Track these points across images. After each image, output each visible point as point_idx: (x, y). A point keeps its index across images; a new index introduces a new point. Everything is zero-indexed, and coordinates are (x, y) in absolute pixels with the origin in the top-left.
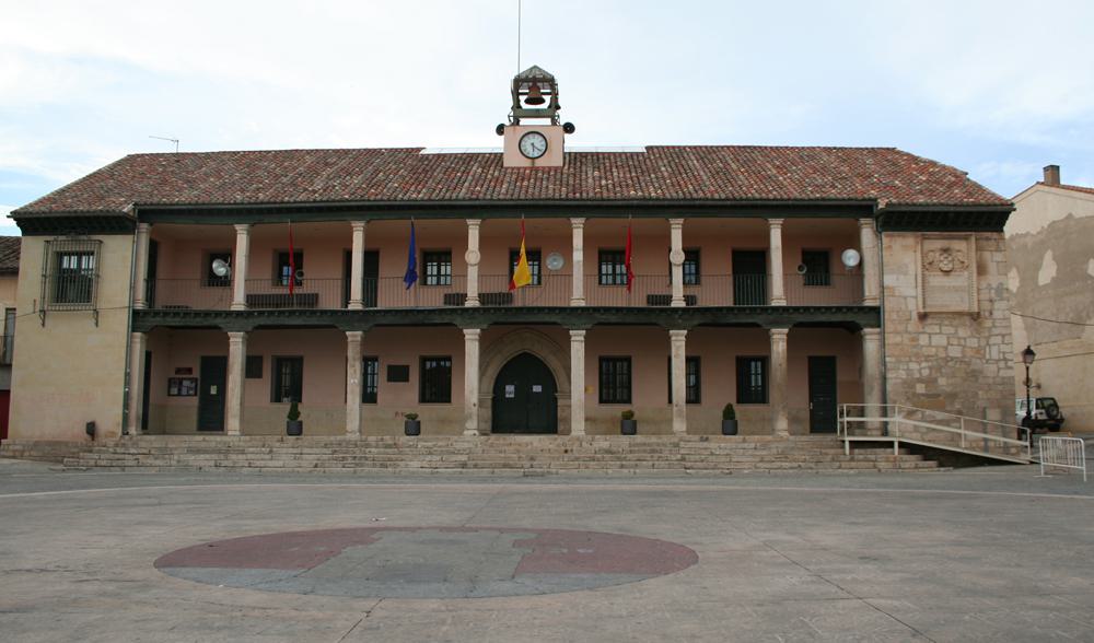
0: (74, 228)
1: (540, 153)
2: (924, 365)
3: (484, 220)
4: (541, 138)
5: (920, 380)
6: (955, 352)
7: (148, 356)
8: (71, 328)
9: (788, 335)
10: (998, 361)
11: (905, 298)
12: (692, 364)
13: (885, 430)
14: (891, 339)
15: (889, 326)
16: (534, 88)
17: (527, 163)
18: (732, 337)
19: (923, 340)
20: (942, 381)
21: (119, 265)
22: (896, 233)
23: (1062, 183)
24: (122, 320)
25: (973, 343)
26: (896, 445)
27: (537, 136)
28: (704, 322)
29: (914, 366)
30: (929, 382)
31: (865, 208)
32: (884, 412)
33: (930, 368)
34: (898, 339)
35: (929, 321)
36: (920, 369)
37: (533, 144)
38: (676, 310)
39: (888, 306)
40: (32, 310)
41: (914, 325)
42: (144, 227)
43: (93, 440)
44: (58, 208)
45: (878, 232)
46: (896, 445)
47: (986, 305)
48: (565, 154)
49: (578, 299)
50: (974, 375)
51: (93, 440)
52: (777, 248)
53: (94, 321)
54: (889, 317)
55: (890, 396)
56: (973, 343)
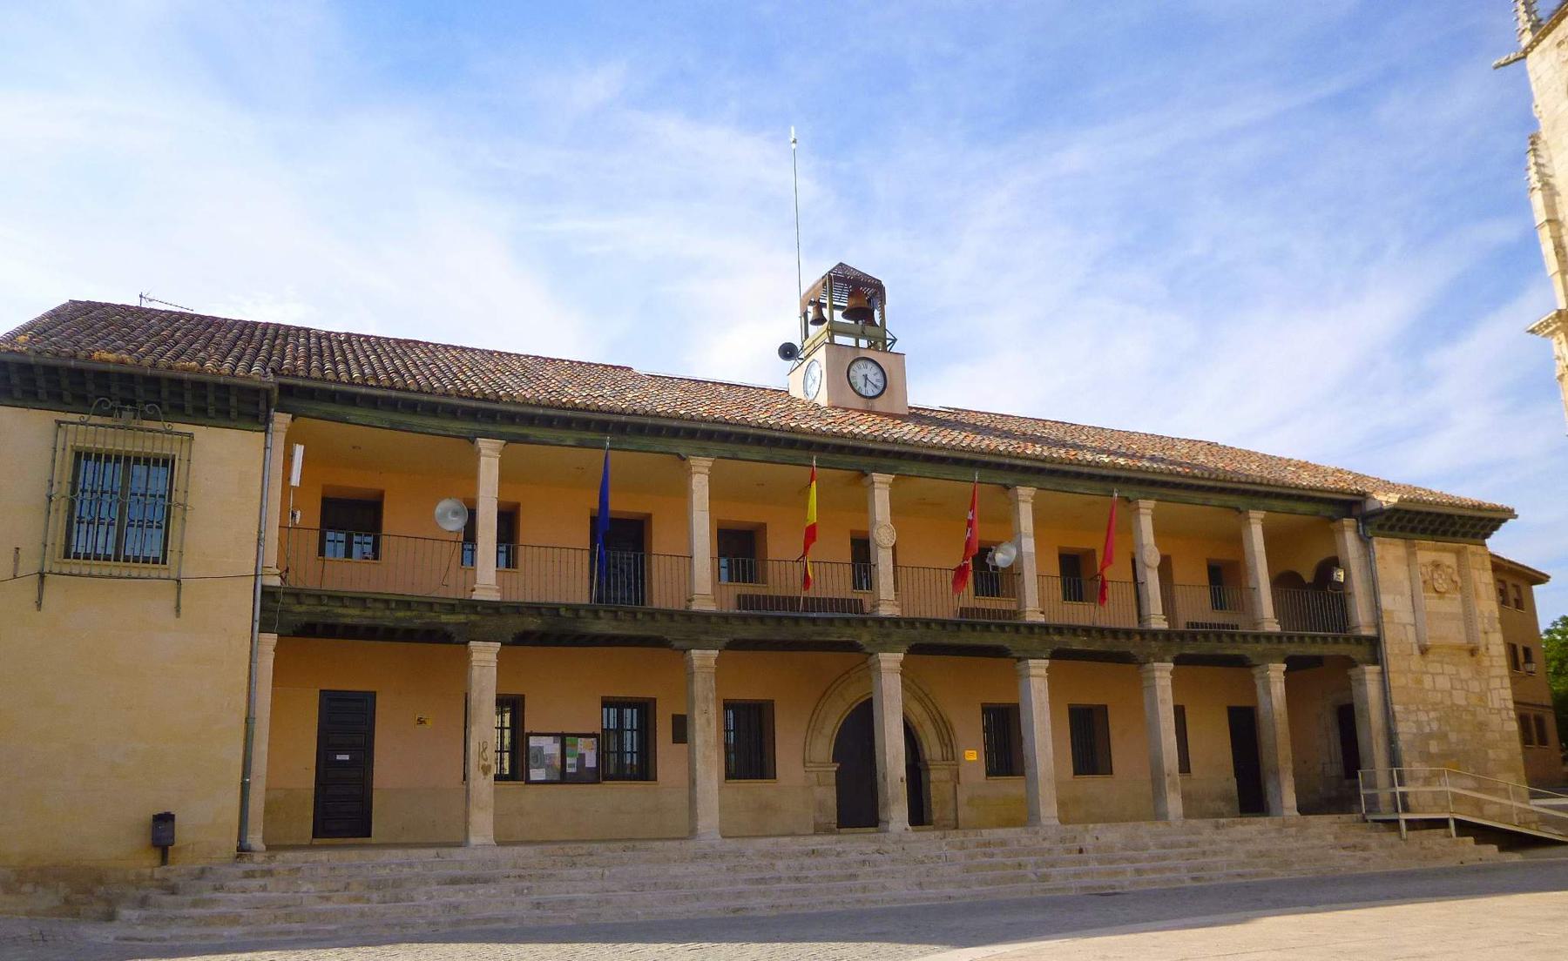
0: (133, 403)
1: (877, 392)
2: (1432, 714)
3: (901, 476)
4: (875, 369)
5: (1431, 736)
7: (1180, 712)
8: (109, 616)
9: (1048, 670)
10: (1499, 711)
11: (1404, 626)
14: (1396, 681)
15: (1394, 662)
16: (856, 299)
19: (1427, 682)
20: (1453, 737)
21: (235, 489)
22: (1387, 540)
24: (242, 606)
25: (1475, 686)
26: (1452, 823)
27: (870, 365)
28: (537, 632)
29: (1423, 717)
30: (1443, 737)
33: (1439, 719)
34: (1403, 681)
35: (1430, 657)
36: (1430, 721)
37: (866, 377)
39: (1389, 634)
41: (1416, 662)
42: (281, 421)
43: (164, 860)
45: (1365, 541)
46: (1452, 823)
47: (1482, 642)
48: (266, 431)
50: (1482, 726)
51: (164, 860)
52: (1029, 554)
53: (34, 596)
54: (1391, 649)
56: (1475, 686)
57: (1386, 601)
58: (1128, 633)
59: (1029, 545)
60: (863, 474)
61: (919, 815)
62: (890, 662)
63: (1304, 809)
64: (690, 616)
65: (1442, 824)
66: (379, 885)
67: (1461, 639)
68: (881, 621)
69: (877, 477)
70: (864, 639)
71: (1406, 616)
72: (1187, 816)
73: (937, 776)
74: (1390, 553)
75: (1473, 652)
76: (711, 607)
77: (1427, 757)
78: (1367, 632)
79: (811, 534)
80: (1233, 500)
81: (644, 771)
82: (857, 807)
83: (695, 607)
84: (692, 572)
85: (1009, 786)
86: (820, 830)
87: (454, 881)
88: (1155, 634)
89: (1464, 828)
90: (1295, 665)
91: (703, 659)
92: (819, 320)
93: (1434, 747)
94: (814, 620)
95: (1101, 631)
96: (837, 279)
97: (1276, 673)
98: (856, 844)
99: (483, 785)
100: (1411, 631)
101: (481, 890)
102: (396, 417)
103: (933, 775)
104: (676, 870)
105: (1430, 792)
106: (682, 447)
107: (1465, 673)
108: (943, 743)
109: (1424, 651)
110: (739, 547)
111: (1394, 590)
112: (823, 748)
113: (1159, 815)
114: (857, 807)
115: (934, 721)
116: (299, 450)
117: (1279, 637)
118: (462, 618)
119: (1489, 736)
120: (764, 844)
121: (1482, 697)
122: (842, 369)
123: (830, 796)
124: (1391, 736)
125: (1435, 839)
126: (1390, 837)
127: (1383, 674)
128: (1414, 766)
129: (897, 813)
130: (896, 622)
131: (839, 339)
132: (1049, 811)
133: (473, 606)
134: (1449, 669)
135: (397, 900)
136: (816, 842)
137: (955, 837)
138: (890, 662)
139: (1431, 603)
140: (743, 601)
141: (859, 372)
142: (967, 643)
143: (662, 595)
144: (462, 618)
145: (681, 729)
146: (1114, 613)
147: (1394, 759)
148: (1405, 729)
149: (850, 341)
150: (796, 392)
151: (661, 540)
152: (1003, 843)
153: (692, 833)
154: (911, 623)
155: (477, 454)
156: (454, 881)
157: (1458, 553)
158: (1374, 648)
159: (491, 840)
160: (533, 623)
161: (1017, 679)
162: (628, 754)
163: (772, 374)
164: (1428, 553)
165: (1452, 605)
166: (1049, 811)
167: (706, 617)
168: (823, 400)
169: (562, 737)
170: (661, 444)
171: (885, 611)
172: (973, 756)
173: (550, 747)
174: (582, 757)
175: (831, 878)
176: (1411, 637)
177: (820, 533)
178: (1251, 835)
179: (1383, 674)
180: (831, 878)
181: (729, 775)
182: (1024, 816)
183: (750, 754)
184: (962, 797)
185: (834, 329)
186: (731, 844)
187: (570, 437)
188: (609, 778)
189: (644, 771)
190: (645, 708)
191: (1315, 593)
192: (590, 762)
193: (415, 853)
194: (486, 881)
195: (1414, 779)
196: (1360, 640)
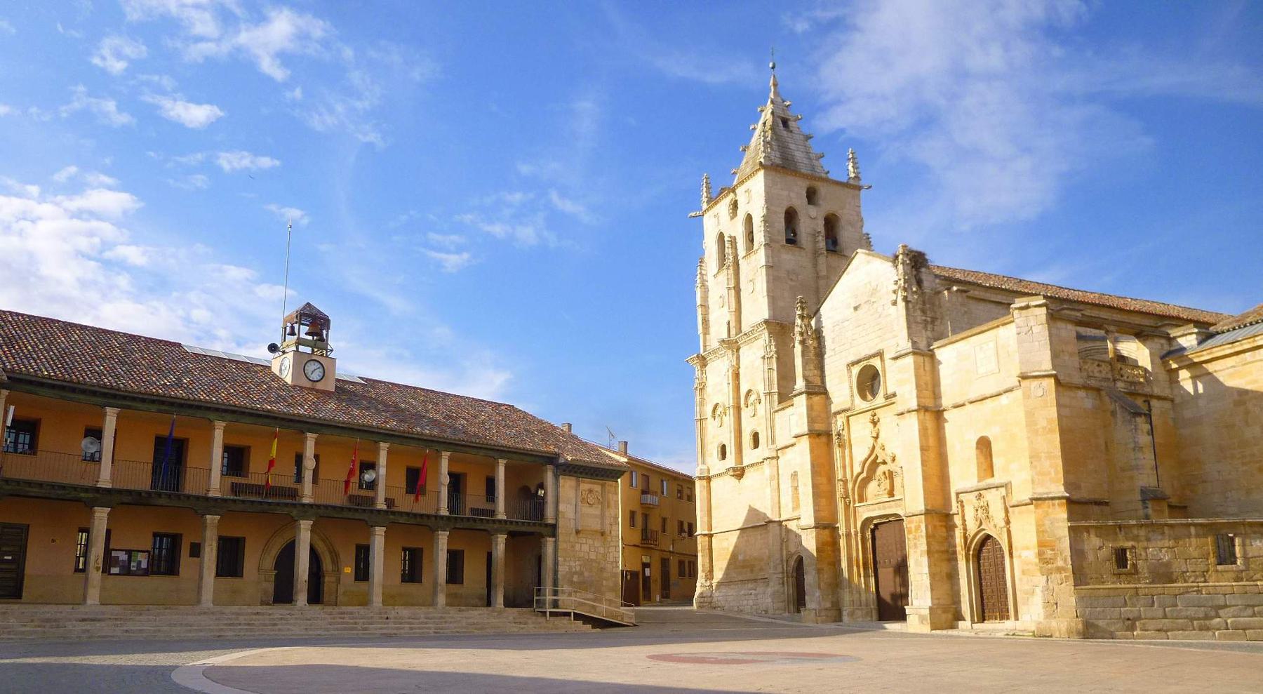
5: (576, 573)
6: (593, 556)
7: (108, 532)
12: (816, 399)
13: (555, 604)
14: (561, 545)
15: (561, 538)
17: (309, 385)
18: (471, 526)
19: (577, 547)
20: (586, 574)
23: (947, 354)
25: (602, 550)
28: (123, 501)
29: (572, 564)
30: (581, 574)
31: (552, 459)
32: (555, 593)
36: (576, 566)
38: (379, 511)
39: (561, 523)
40: (714, 483)
41: (573, 538)
44: (394, 398)
45: (556, 477)
49: (105, 479)
50: (602, 570)
54: (561, 531)
55: (560, 582)
56: (602, 550)
57: (562, 507)
58: (429, 516)
59: (382, 471)
60: (303, 432)
61: (315, 597)
62: (305, 526)
63: (506, 605)
64: (207, 499)
65: (568, 614)
66: (48, 620)
67: (598, 527)
68: (304, 505)
69: (309, 435)
70: (294, 513)
71: (571, 515)
72: (447, 604)
73: (328, 580)
74: (568, 486)
75: (603, 534)
76: (219, 495)
77: (571, 583)
78: (550, 521)
79: (271, 463)
80: (491, 453)
81: (171, 569)
82: (283, 594)
83: (211, 495)
84: (209, 473)
85: (362, 586)
86: (263, 603)
87: (84, 620)
88: (442, 517)
89: (578, 617)
90: (512, 535)
91: (212, 519)
92: (293, 333)
93: (575, 579)
94: (270, 504)
95: (415, 515)
96: (305, 315)
97: (501, 540)
98: (279, 611)
99: (95, 576)
100: (573, 522)
101: (98, 624)
102: (64, 394)
103: (327, 579)
104: (191, 619)
105: (570, 600)
106: (212, 416)
107: (597, 544)
108: (333, 562)
109: (578, 532)
110: (236, 459)
111: (566, 500)
112: (269, 562)
113: (433, 604)
114: (283, 594)
115: (330, 553)
116: (12, 408)
117: (506, 522)
118: (91, 495)
119: (605, 575)
120: (235, 609)
121: (604, 555)
122: (301, 363)
123: (270, 587)
124: (556, 572)
125: (565, 620)
126: (542, 620)
127: (556, 542)
128: (564, 587)
129: (302, 598)
130: (311, 506)
131: (302, 348)
132: (377, 599)
133: (98, 490)
134: (590, 542)
135: (58, 627)
136: (259, 609)
137: (329, 609)
138: (305, 526)
139: (586, 510)
140: (235, 489)
141: (311, 367)
142: (351, 517)
143: (191, 486)
144: (91, 495)
145: (196, 551)
146: (423, 506)
147: (555, 583)
148: (562, 569)
149: (309, 350)
150: (275, 370)
151: (193, 458)
152: (351, 613)
153: (199, 602)
154: (318, 506)
155: (105, 414)
156: (84, 620)
157: (603, 486)
158: (553, 530)
159: (97, 602)
160: (126, 499)
161: (370, 535)
162: (166, 561)
163: (260, 354)
164: (586, 485)
165: (596, 511)
166: (377, 599)
167: (216, 499)
168: (289, 380)
169: (129, 553)
170: (199, 413)
171: (306, 500)
172: (348, 570)
173: (123, 556)
174: (139, 563)
175: (265, 625)
176: (572, 525)
177: (276, 464)
178: (478, 615)
179: (556, 542)
180: (265, 625)
181: (218, 574)
182: (365, 602)
183: (230, 563)
184: (341, 590)
185: (300, 342)
186: (218, 608)
187: (154, 408)
188: (153, 573)
189: (171, 569)
190: (175, 540)
191: (529, 498)
192: (144, 565)
193: (61, 608)
194: (99, 620)
195: (563, 592)
196: (547, 525)
